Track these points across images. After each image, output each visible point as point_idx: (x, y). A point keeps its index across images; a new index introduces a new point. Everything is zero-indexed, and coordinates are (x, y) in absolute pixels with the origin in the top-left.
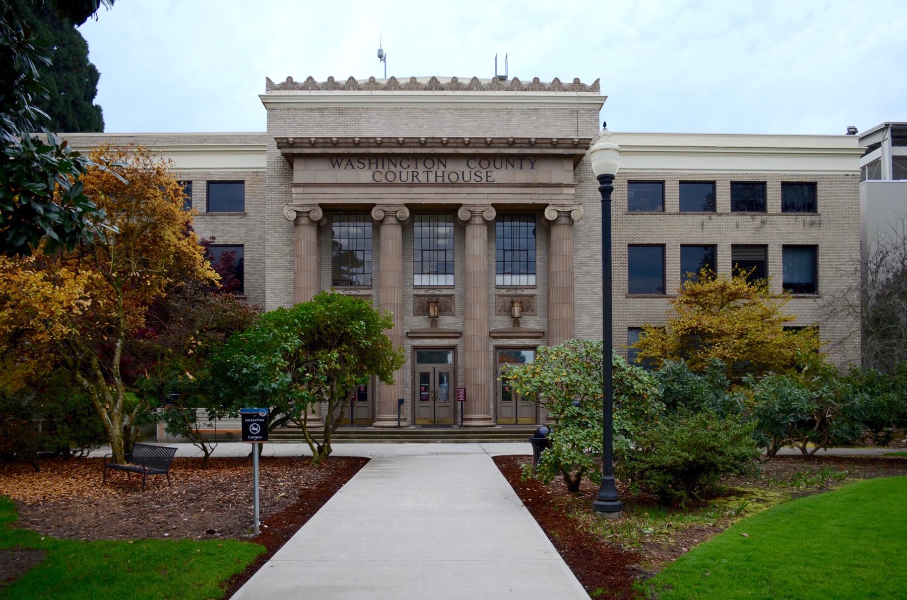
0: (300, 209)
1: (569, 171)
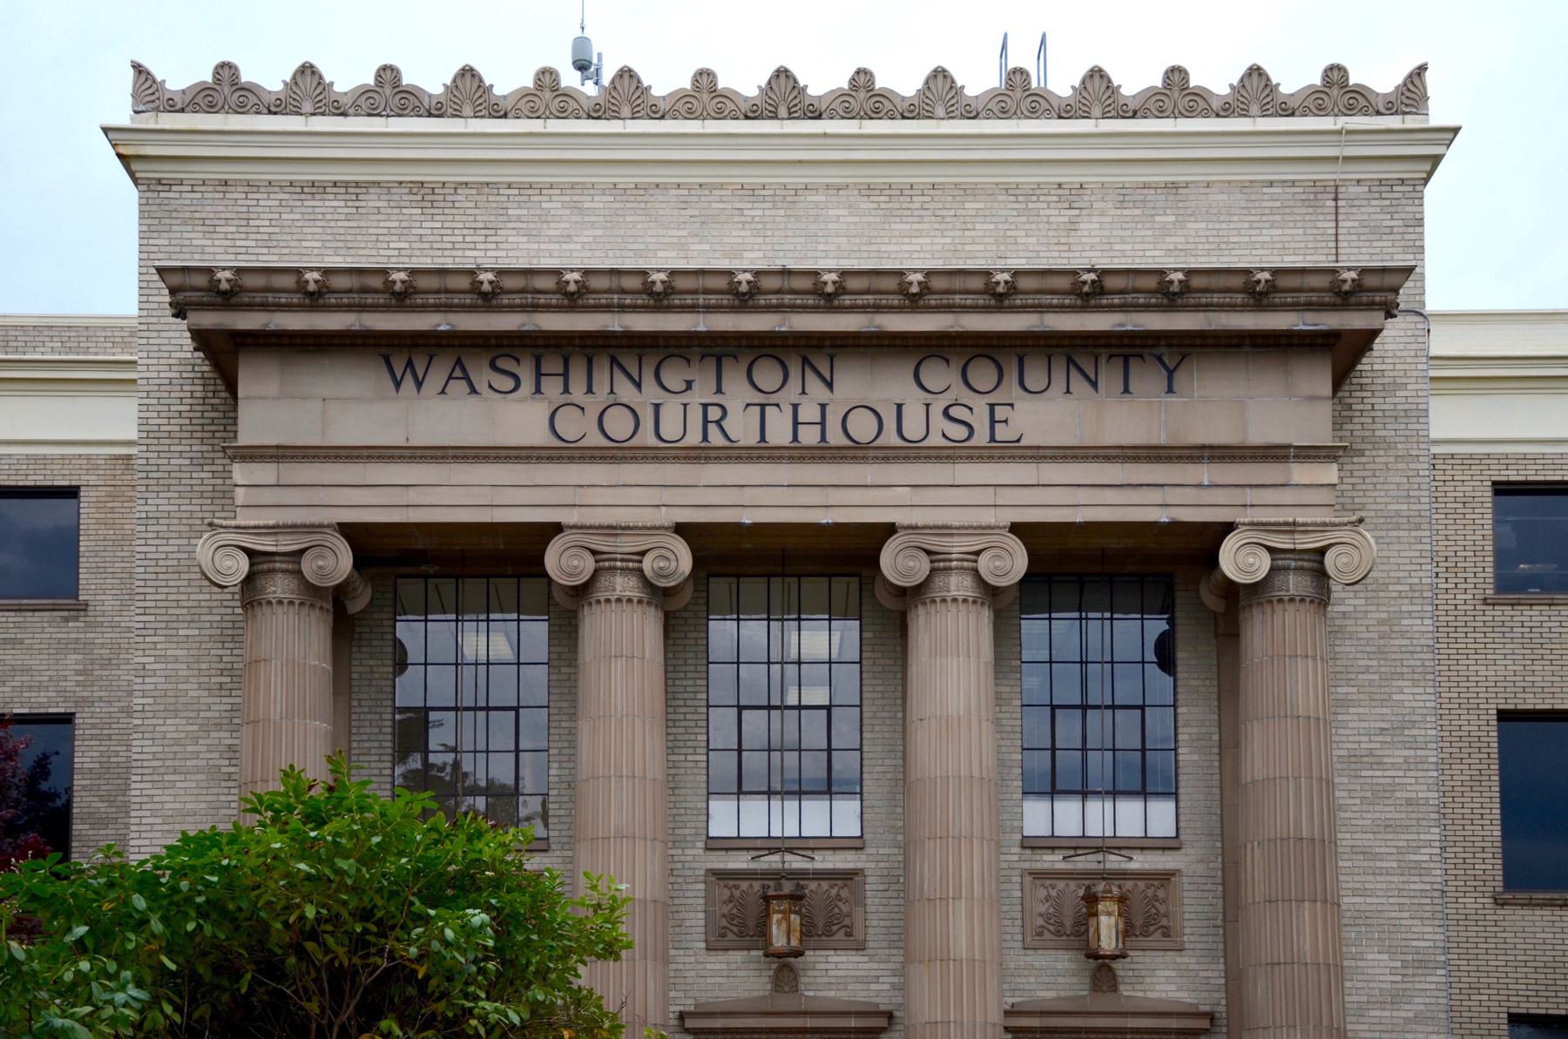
0: (265, 544)
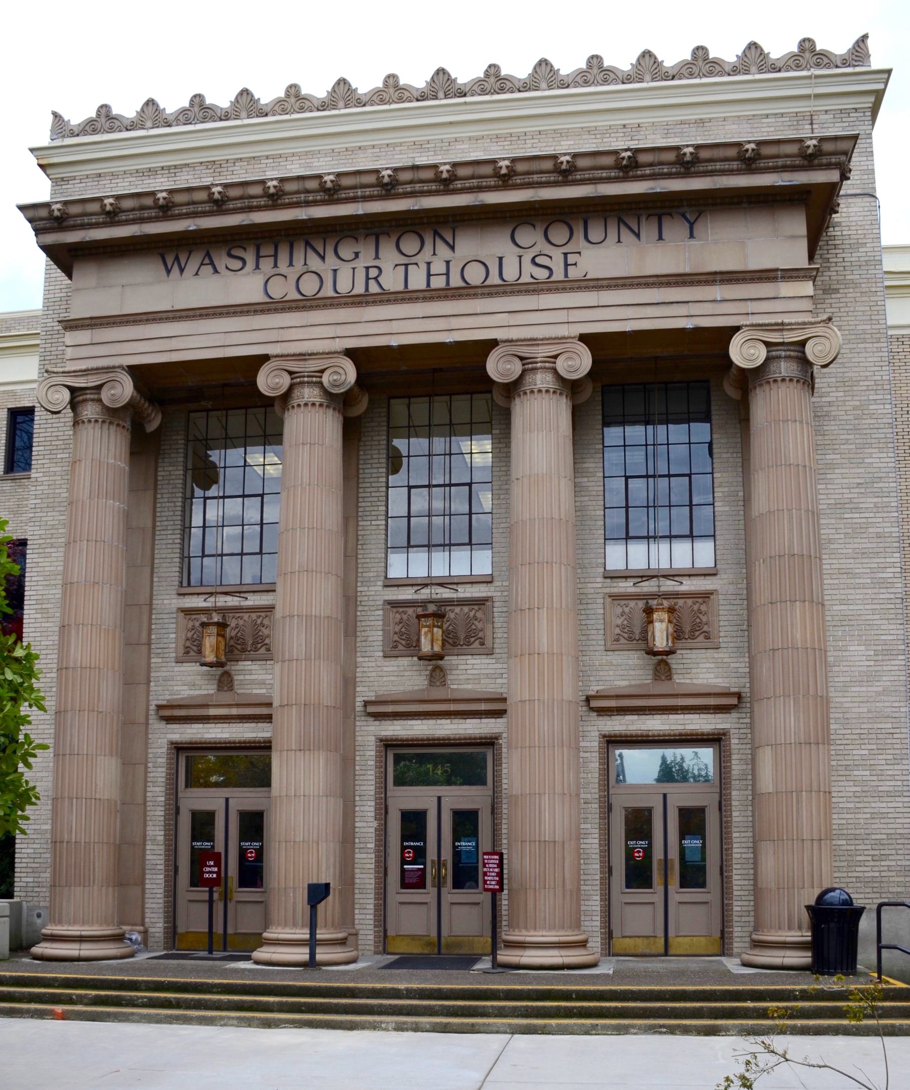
1: (793, 237)
